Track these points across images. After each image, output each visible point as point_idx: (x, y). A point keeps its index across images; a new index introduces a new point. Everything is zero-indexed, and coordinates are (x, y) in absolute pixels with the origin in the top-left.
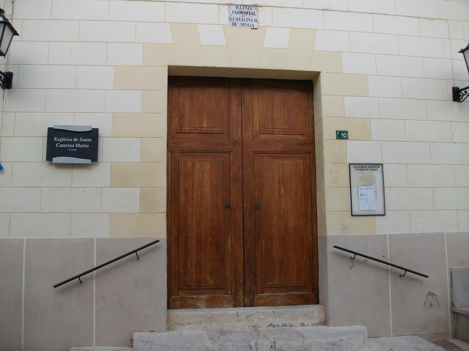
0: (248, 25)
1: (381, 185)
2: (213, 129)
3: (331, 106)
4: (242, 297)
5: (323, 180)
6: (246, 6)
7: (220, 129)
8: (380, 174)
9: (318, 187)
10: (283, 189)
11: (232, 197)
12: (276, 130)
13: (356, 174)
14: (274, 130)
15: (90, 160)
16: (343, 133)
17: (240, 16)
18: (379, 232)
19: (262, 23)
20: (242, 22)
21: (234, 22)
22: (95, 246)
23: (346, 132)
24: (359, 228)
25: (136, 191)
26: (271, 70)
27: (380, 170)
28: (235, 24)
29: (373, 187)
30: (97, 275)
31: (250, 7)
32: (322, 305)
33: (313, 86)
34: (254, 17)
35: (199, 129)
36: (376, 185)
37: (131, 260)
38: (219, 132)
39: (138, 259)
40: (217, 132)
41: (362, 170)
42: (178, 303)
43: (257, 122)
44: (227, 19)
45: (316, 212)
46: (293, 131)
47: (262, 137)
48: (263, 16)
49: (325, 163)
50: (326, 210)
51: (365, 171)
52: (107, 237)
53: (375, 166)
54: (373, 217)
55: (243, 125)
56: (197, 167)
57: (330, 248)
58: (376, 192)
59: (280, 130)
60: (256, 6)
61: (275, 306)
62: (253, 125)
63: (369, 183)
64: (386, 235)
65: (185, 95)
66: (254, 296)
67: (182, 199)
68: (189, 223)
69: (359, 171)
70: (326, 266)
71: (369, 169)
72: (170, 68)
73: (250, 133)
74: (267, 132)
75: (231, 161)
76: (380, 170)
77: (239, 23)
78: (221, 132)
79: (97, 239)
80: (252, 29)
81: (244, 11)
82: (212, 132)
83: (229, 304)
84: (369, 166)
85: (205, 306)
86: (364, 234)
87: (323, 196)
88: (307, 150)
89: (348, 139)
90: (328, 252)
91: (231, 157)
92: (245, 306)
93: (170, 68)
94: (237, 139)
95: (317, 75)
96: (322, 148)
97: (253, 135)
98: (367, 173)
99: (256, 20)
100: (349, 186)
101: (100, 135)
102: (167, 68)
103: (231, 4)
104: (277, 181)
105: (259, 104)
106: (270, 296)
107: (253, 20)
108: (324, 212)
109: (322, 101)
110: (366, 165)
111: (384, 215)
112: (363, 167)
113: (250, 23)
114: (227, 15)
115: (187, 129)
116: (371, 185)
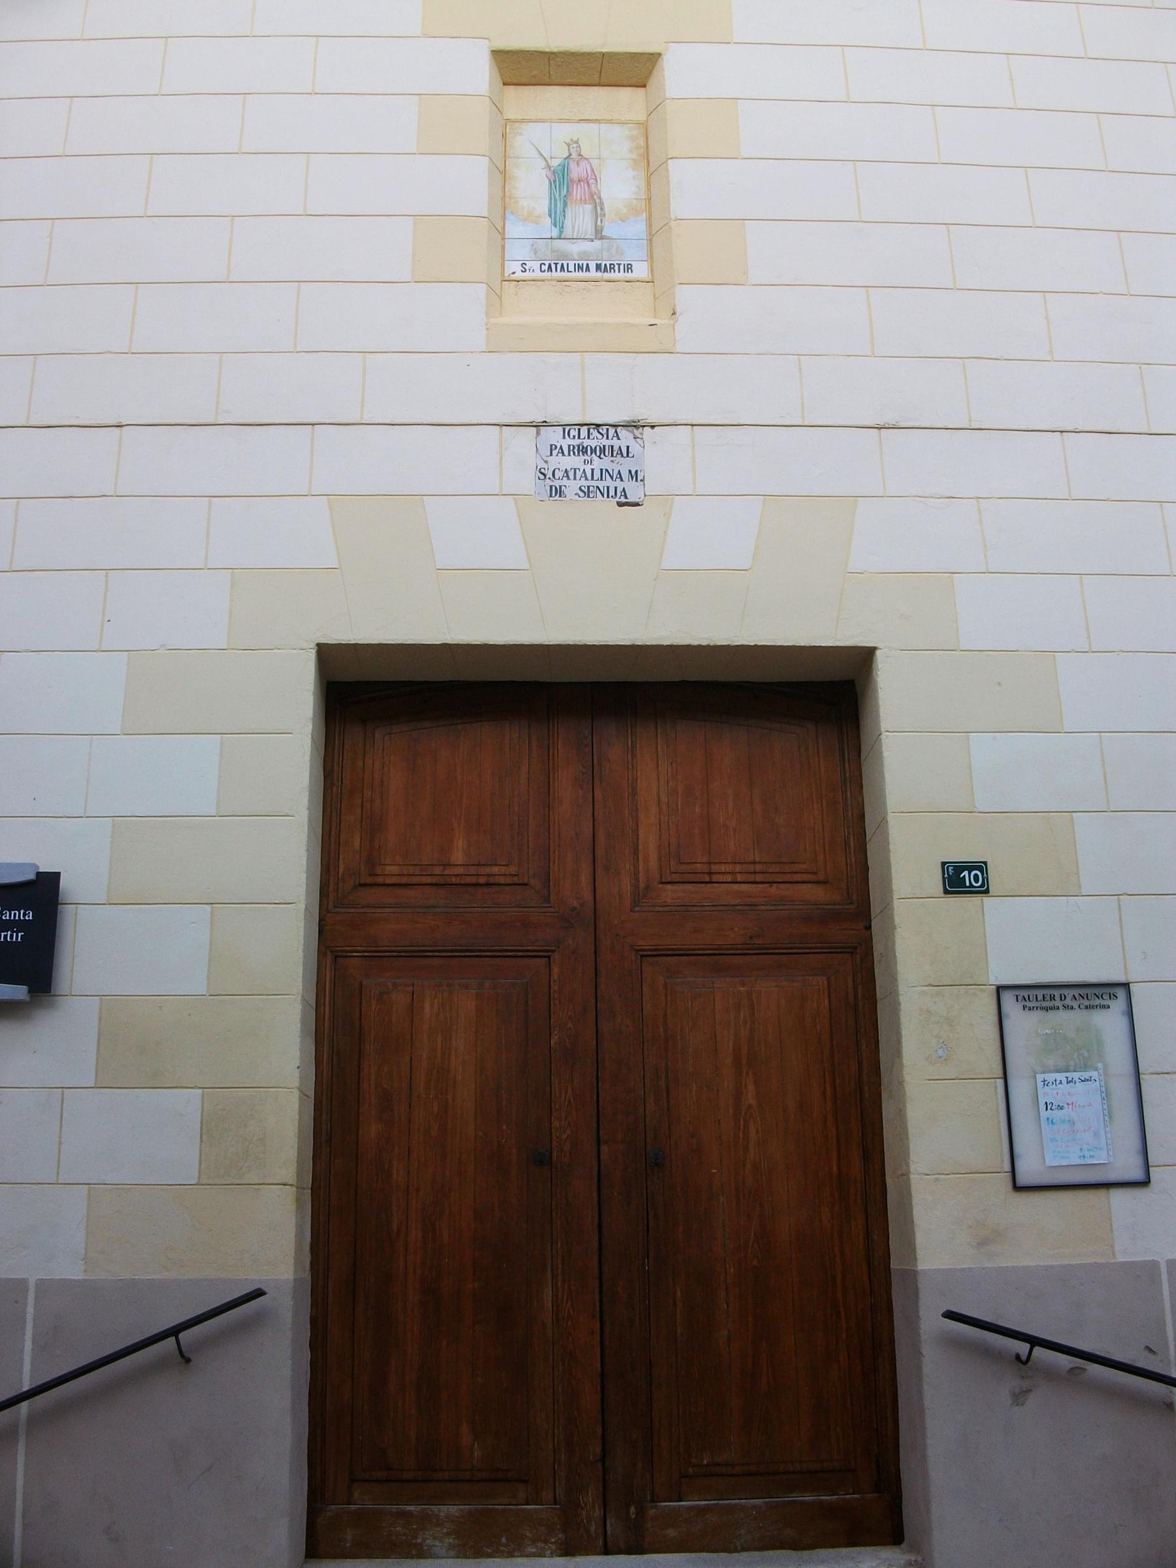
0: (606, 493)
1: (1126, 1066)
2: (488, 870)
3: (926, 773)
4: (598, 1513)
5: (898, 1053)
6: (598, 426)
7: (512, 870)
8: (1122, 1023)
9: (885, 1080)
10: (751, 1087)
11: (556, 1124)
12: (723, 868)
13: (1024, 1025)
14: (714, 868)
15: (24, 988)
16: (970, 870)
17: (576, 461)
18: (1127, 1251)
19: (654, 483)
20: (583, 482)
21: (557, 483)
22: (30, 1310)
23: (982, 867)
24: (1044, 1238)
25: (188, 1102)
26: (688, 647)
27: (1118, 1005)
28: (559, 492)
29: (1094, 1074)
30: (34, 1420)
31: (612, 431)
32: (915, 1548)
33: (856, 703)
34: (625, 465)
35: (438, 870)
36: (1105, 1067)
37: (159, 1366)
38: (509, 880)
39: (188, 1361)
40: (502, 880)
41: (1047, 1009)
42: (349, 1535)
43: (649, 842)
44: (531, 475)
45: (884, 1175)
46: (787, 868)
47: (670, 894)
48: (657, 457)
49: (902, 988)
50: (912, 1167)
51: (1062, 1015)
52: (75, 1272)
53: (1097, 991)
54: (1101, 1194)
55: (600, 852)
56: (427, 1009)
57: (931, 1322)
58: (1107, 1095)
59: (738, 868)
60: (633, 425)
61: (724, 1551)
62: (636, 852)
63: (1079, 1058)
64: (1154, 1264)
65: (388, 754)
66: (641, 1511)
67: (372, 1130)
68: (395, 1228)
69: (1036, 1016)
70: (920, 1392)
71: (1075, 1004)
72: (327, 655)
73: (627, 885)
74: (691, 877)
75: (555, 987)
76: (1118, 1005)
77: (572, 487)
78: (516, 880)
79: (40, 1283)
80: (620, 504)
81: (593, 443)
82: (482, 880)
83: (546, 1542)
84: (1076, 992)
85: (451, 1547)
86: (1066, 1262)
87: (901, 1113)
88: (835, 941)
89: (987, 892)
90: (923, 1337)
91: (556, 970)
92: (606, 1551)
93: (327, 655)
94: (576, 904)
95: (864, 657)
96: (890, 928)
97: (636, 887)
98: (1067, 1020)
99: (634, 475)
100: (1000, 1073)
101: (62, 897)
102: (314, 652)
103: (545, 424)
104: (729, 1061)
105: (655, 770)
106: (701, 1511)
107: (625, 475)
108: (906, 1175)
109: (886, 754)
110: (1065, 992)
111: (1145, 1183)
112: (1052, 998)
113: (612, 485)
114: (533, 462)
115: (391, 870)
116: (1085, 1067)
